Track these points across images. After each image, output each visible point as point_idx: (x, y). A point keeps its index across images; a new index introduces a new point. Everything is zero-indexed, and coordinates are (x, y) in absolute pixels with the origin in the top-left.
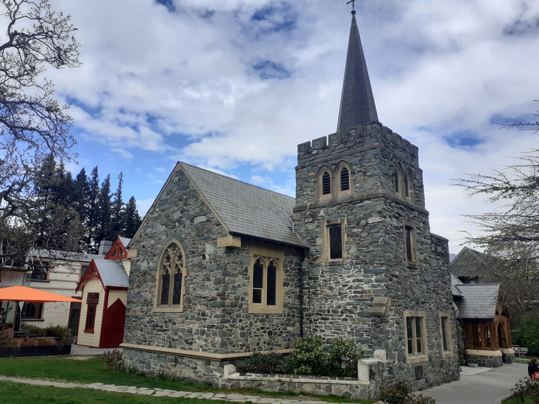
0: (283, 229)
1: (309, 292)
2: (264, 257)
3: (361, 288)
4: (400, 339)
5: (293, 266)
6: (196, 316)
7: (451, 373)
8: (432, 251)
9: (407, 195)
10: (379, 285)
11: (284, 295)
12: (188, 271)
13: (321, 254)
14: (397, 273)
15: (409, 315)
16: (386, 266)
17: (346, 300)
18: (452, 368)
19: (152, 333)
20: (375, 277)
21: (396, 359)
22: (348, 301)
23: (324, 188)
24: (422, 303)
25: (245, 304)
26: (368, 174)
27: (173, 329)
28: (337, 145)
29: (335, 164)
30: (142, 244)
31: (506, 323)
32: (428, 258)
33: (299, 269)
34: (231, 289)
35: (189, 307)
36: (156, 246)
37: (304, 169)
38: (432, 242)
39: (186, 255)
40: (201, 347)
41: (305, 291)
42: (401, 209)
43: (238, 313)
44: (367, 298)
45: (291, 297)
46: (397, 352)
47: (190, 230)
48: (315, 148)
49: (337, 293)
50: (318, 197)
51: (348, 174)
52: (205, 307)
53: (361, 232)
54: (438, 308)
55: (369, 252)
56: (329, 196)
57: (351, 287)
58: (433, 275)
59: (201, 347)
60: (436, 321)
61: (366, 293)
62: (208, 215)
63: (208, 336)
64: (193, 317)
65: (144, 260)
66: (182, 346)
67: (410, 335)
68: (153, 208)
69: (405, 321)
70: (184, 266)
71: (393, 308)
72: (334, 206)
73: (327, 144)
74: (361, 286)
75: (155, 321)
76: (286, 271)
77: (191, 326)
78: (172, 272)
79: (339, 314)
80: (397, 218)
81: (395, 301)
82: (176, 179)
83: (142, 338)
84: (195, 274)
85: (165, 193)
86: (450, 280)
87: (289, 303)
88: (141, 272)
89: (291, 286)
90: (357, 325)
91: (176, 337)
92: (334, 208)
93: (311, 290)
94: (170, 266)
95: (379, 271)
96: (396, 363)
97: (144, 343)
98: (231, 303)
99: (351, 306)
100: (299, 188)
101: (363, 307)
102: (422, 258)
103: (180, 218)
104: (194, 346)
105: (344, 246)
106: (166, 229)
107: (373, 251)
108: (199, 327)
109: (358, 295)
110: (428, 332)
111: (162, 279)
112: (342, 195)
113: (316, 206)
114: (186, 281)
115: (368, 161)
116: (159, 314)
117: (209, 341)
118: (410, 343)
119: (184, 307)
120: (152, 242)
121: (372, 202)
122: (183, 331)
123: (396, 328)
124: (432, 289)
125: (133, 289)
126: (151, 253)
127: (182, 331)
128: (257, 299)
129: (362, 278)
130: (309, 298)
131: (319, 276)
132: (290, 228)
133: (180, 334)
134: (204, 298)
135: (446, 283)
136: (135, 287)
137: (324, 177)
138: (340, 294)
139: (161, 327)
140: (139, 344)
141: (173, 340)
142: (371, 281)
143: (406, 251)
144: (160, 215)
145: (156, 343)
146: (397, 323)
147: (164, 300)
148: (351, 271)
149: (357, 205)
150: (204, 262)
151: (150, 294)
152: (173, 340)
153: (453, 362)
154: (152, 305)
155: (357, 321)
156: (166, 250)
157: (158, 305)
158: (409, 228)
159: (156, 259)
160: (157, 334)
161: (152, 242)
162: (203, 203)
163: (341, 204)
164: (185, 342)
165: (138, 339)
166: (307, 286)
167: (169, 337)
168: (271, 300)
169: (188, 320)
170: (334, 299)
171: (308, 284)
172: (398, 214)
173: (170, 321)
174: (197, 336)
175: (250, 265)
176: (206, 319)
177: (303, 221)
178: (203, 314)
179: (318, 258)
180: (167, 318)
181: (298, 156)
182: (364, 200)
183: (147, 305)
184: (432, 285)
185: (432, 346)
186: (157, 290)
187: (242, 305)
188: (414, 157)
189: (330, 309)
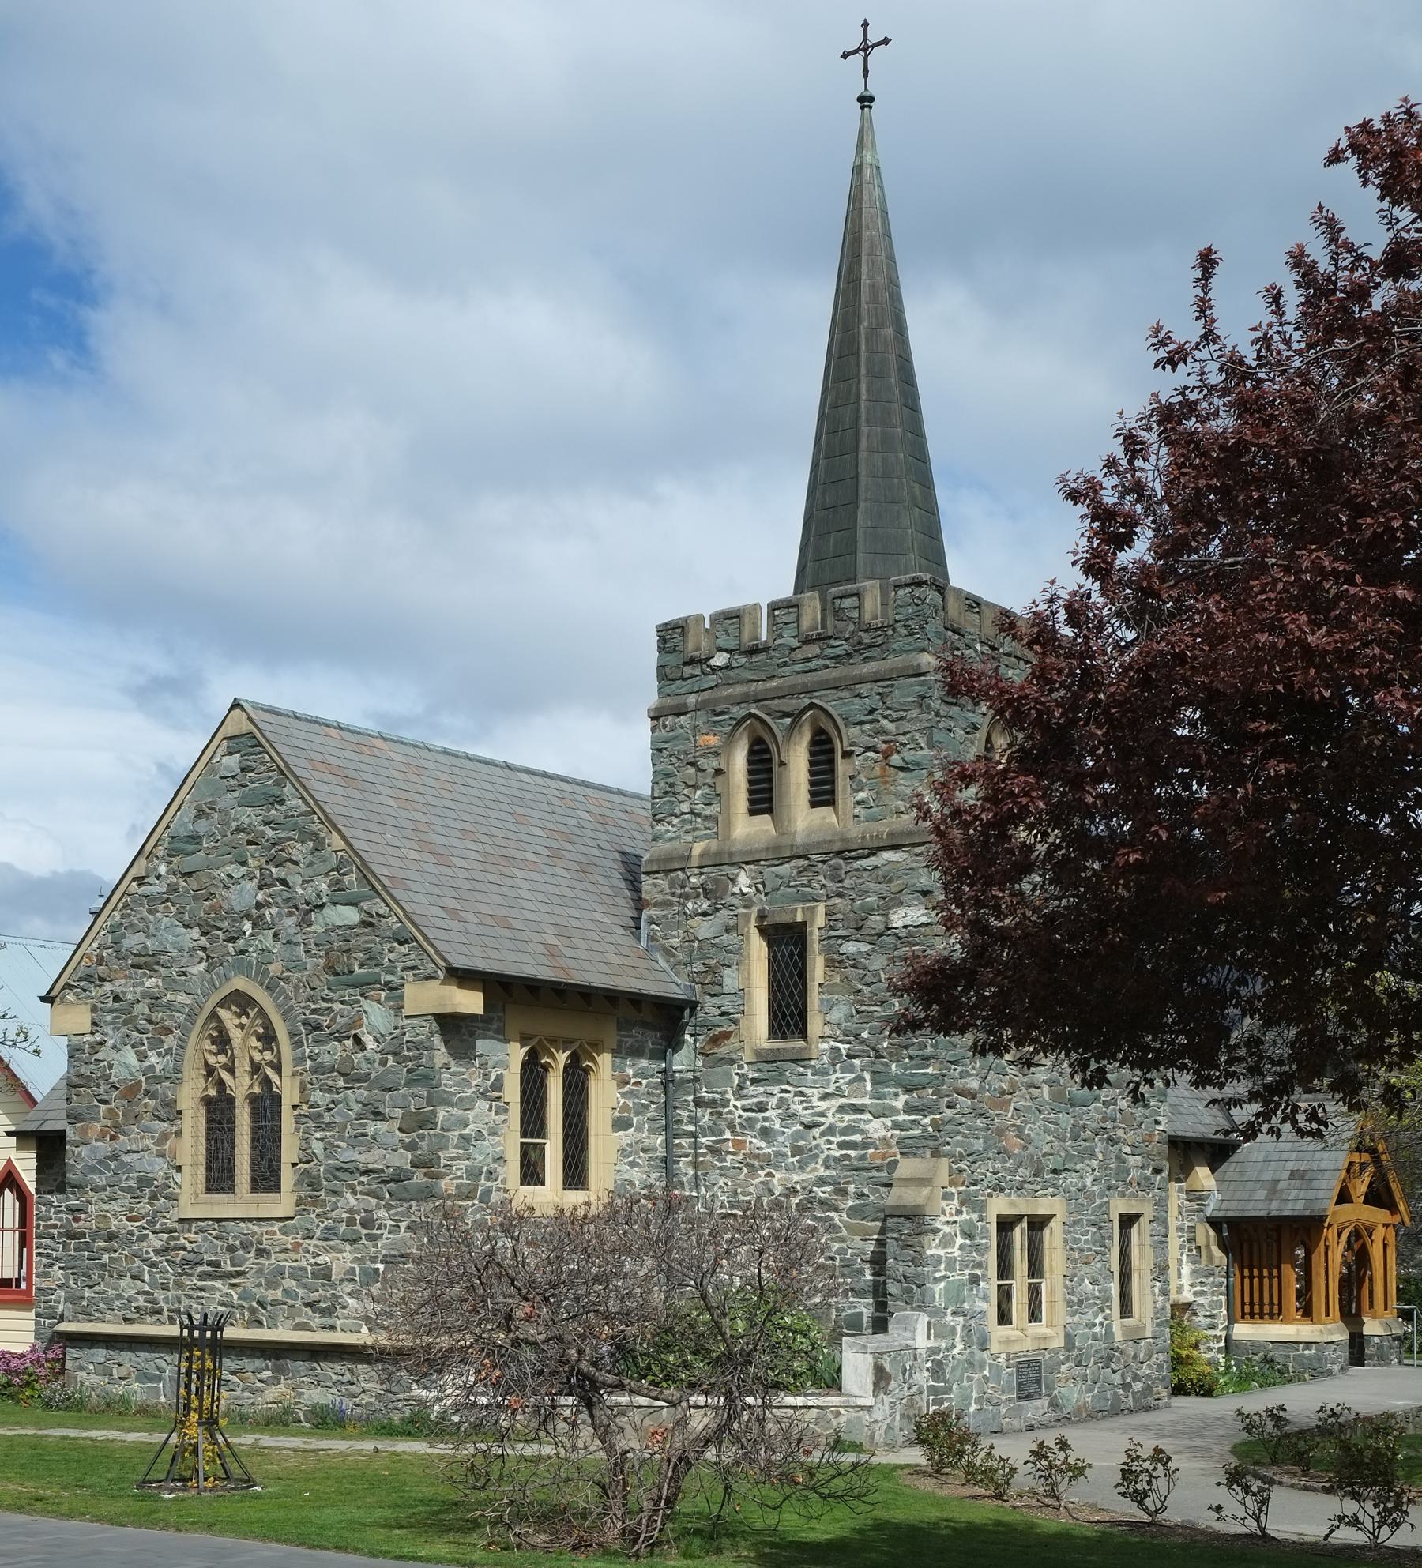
1: (696, 1145)
3: (862, 1132)
4: (974, 1280)
6: (343, 1227)
7: (1138, 1386)
11: (614, 1156)
12: (303, 1090)
14: (974, 1084)
16: (938, 1065)
18: (1145, 1370)
19: (179, 1285)
21: (958, 1338)
22: (822, 1172)
23: (751, 792)
24: (1055, 1171)
25: (498, 1190)
26: (896, 759)
27: (260, 1272)
28: (795, 643)
29: (786, 715)
33: (664, 1072)
34: (456, 1147)
36: (170, 996)
39: (292, 1034)
41: (684, 1142)
45: (637, 1165)
46: (961, 1319)
49: (788, 1151)
50: (728, 825)
52: (374, 1201)
57: (831, 1130)
61: (876, 1147)
62: (366, 905)
64: (329, 1234)
67: (1005, 1269)
68: (142, 861)
69: (993, 1228)
70: (288, 1068)
71: (953, 1190)
73: (764, 637)
74: (862, 1126)
78: (242, 1086)
81: (961, 1171)
82: (233, 762)
87: (632, 1183)
89: (639, 1129)
90: (844, 1245)
91: (278, 1294)
92: (785, 869)
93: (703, 1140)
94: (231, 1070)
95: (916, 1081)
96: (955, 1351)
98: (458, 1186)
99: (829, 1189)
100: (662, 784)
101: (866, 1191)
103: (259, 906)
105: (815, 999)
106: (204, 941)
109: (853, 1153)
112: (805, 820)
113: (729, 860)
115: (895, 715)
118: (1005, 1295)
122: (297, 1275)
123: (961, 1248)
128: (532, 1173)
129: (867, 1101)
130: (695, 1165)
131: (730, 1096)
138: (797, 1151)
141: (261, 1304)
142: (889, 1111)
144: (173, 889)
146: (968, 1235)
147: (219, 1178)
148: (833, 1078)
149: (858, 864)
151: (160, 1160)
152: (261, 1304)
154: (173, 1198)
155: (844, 1233)
156: (213, 1015)
159: (170, 1041)
163: (805, 857)
165: (126, 1307)
166: (691, 1128)
168: (575, 1175)
169: (315, 1242)
170: (778, 1168)
171: (694, 1121)
173: (245, 1246)
174: (349, 1287)
175: (507, 1067)
179: (727, 1036)
181: (661, 667)
183: (154, 1197)
185: (1080, 1303)
186: (191, 1143)
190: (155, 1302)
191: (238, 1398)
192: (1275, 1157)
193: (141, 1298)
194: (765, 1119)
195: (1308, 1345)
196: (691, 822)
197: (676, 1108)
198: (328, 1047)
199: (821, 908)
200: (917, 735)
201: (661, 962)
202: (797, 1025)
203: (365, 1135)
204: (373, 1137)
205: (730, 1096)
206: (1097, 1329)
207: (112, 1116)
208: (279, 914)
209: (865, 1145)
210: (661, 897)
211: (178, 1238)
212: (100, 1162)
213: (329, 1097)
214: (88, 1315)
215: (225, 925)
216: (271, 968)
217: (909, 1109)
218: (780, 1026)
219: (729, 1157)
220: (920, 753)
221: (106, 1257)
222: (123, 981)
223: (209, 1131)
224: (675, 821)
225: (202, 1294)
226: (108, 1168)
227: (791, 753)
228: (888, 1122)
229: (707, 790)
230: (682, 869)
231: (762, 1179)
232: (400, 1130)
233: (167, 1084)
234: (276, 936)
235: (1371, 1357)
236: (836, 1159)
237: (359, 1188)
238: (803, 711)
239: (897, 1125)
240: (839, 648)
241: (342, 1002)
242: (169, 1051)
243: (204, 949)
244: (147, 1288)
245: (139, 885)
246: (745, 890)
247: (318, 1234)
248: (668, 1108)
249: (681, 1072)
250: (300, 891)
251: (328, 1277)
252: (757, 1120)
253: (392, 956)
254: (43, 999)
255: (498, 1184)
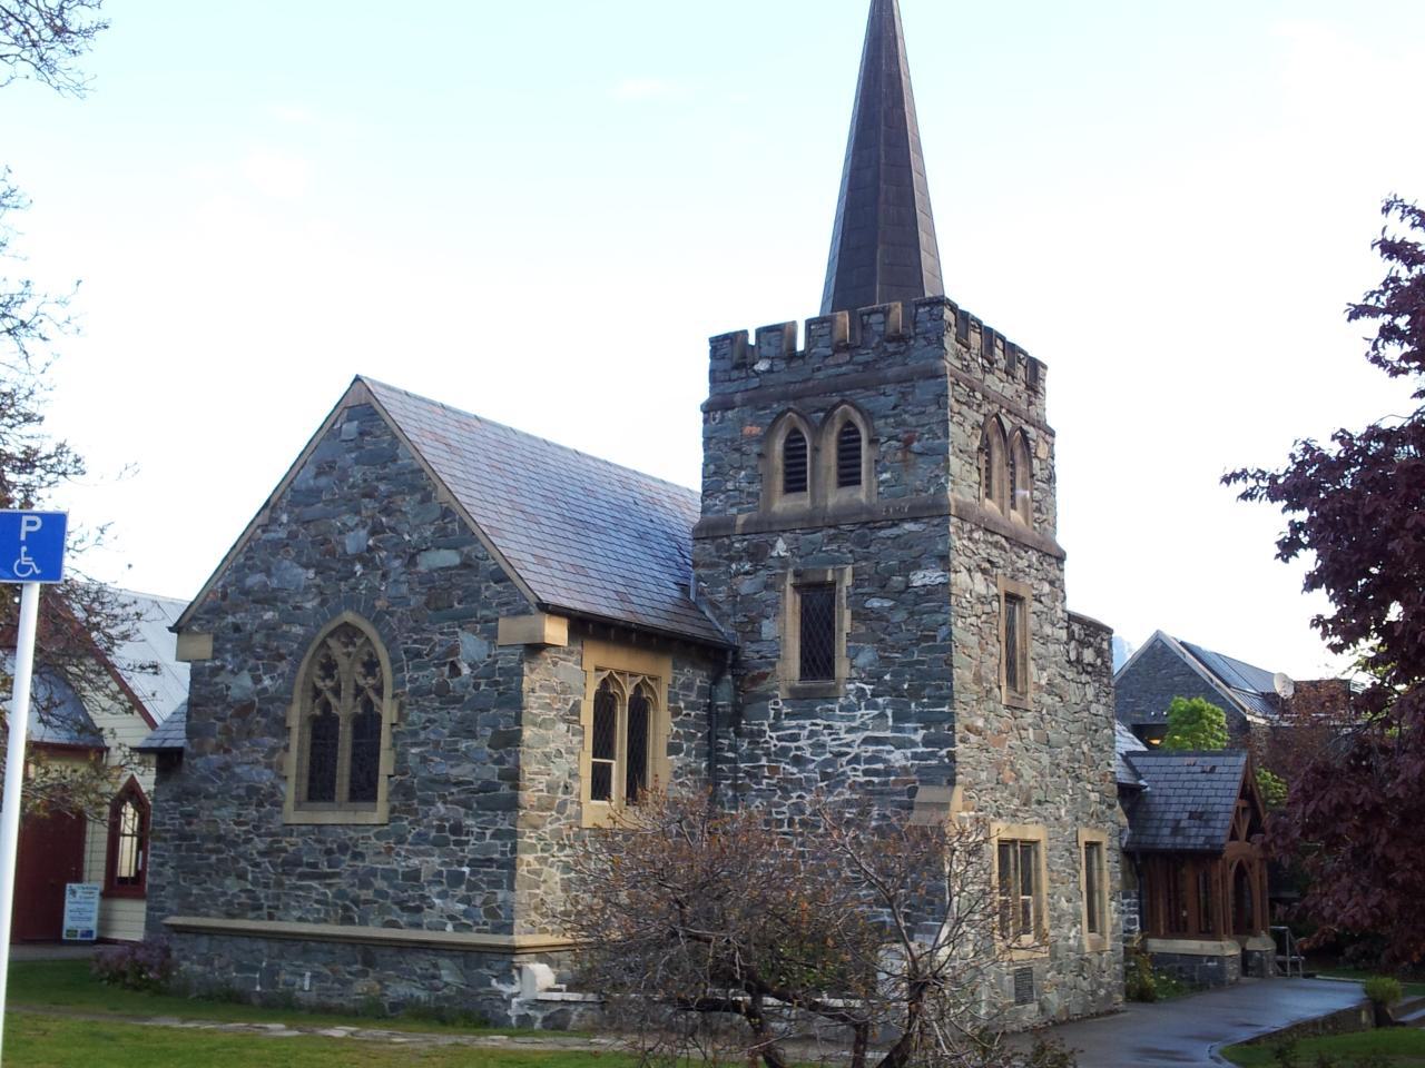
0: (665, 591)
1: (737, 770)
2: (621, 673)
3: (885, 761)
5: (693, 698)
6: (433, 834)
7: (1102, 992)
8: (1069, 662)
9: (1013, 506)
10: (933, 755)
12: (401, 707)
13: (773, 664)
14: (980, 723)
15: (1005, 836)
17: (842, 793)
18: (1106, 979)
19: (280, 884)
20: (922, 733)
22: (847, 795)
24: (1039, 803)
26: (916, 445)
27: (354, 873)
28: (829, 352)
30: (230, 619)
31: (1257, 865)
32: (1058, 680)
33: (709, 706)
35: (410, 811)
36: (285, 628)
37: (730, 414)
38: (1071, 636)
39: (393, 661)
40: (451, 918)
42: (996, 545)
43: (555, 826)
44: (899, 788)
47: (404, 589)
48: (765, 350)
50: (769, 501)
51: (859, 440)
52: (462, 810)
53: (891, 608)
54: (1077, 819)
55: (911, 664)
56: (801, 502)
57: (856, 759)
58: (1071, 727)
59: (451, 918)
60: (1071, 853)
62: (466, 549)
63: (473, 887)
65: (241, 669)
66: (387, 918)
68: (267, 512)
70: (388, 691)
72: (816, 530)
75: (291, 849)
76: (676, 712)
77: (415, 861)
78: (345, 708)
79: (821, 831)
80: (984, 572)
83: (244, 898)
84: (424, 716)
85: (312, 470)
86: (1112, 741)
88: (229, 706)
89: (688, 754)
91: (367, 894)
94: (337, 692)
97: (250, 914)
100: (712, 467)
101: (888, 813)
102: (1043, 682)
103: (369, 549)
104: (428, 917)
105: (842, 646)
106: (318, 580)
107: (923, 663)
108: (444, 864)
109: (876, 780)
110: (1052, 880)
111: (308, 730)
112: (836, 498)
113: (767, 527)
114: (395, 736)
115: (916, 410)
116: (304, 828)
117: (478, 901)
119: (393, 810)
120: (268, 615)
121: (922, 526)
122: (389, 875)
124: (1065, 764)
125: (200, 755)
126: (265, 648)
127: (383, 877)
128: (600, 789)
129: (888, 734)
130: (734, 787)
131: (766, 728)
132: (684, 588)
133: (380, 884)
134: (458, 784)
135: (1101, 750)
136: (208, 748)
137: (788, 441)
138: (825, 777)
139: (314, 865)
140: (231, 916)
141: (356, 902)
143: (1004, 661)
144: (292, 536)
145: (296, 913)
147: (319, 788)
148: (858, 713)
149: (882, 533)
150: (452, 683)
151: (267, 771)
153: (1108, 963)
154: (279, 804)
156: (324, 643)
157: (298, 805)
158: (1013, 599)
159: (284, 666)
160: (300, 888)
161: (268, 615)
162: (447, 513)
163: (835, 527)
164: (395, 907)
165: (229, 903)
167: (341, 894)
169: (407, 846)
171: (733, 748)
172: (989, 561)
173: (343, 848)
176: (467, 842)
177: (723, 569)
178: (457, 829)
179: (764, 676)
180: (332, 842)
182: (903, 520)
183: (260, 804)
184: (1063, 755)
186: (294, 760)
187: (564, 804)
188: (1036, 392)
189: (797, 818)
190: (256, 899)
191: (328, 989)
192: (1174, 800)
193: (243, 895)
194: (798, 748)
195: (1211, 958)
196: (735, 497)
197: (718, 737)
198: (426, 673)
199: (849, 570)
200: (935, 427)
201: (708, 613)
202: (825, 668)
203: (457, 750)
204: (465, 754)
205: (766, 728)
206: (1071, 942)
207: (227, 731)
208: (387, 557)
209: (887, 772)
210: (708, 559)
211: (280, 842)
212: (214, 773)
213: (424, 716)
214: (193, 910)
215: (339, 566)
216: (379, 604)
217: (927, 742)
218: (810, 669)
219: (765, 781)
220: (937, 441)
221: (213, 858)
222: (243, 614)
223: (313, 746)
224: (722, 497)
225: (301, 893)
226: (220, 778)
227: (824, 441)
228: (908, 753)
229: (749, 471)
230: (728, 536)
231: (794, 800)
232: (489, 746)
233: (278, 704)
234: (384, 576)
235: (1253, 969)
236: (861, 784)
237: (449, 798)
238: (835, 407)
239: (915, 756)
240: (865, 355)
241: (441, 634)
242: (282, 675)
243: (318, 586)
244: (250, 887)
245: (264, 532)
246: (782, 554)
247: (410, 837)
248: (710, 738)
249: (722, 706)
250: (407, 538)
251: (417, 878)
252: (790, 749)
253: (487, 594)
254: (171, 629)
255: (572, 797)
